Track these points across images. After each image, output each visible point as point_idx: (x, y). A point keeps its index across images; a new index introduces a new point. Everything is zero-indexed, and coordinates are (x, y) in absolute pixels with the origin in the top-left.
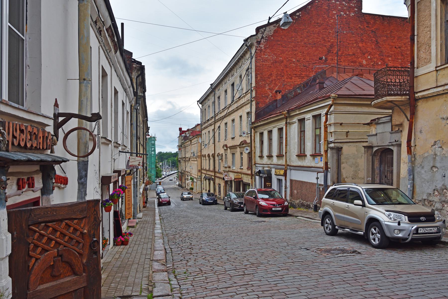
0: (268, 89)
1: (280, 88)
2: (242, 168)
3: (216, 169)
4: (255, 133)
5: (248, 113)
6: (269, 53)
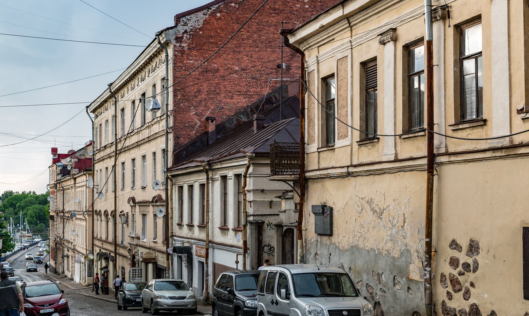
0: (194, 114)
1: (213, 113)
2: (155, 241)
3: (117, 240)
4: (172, 185)
5: (164, 150)
6: (195, 56)
